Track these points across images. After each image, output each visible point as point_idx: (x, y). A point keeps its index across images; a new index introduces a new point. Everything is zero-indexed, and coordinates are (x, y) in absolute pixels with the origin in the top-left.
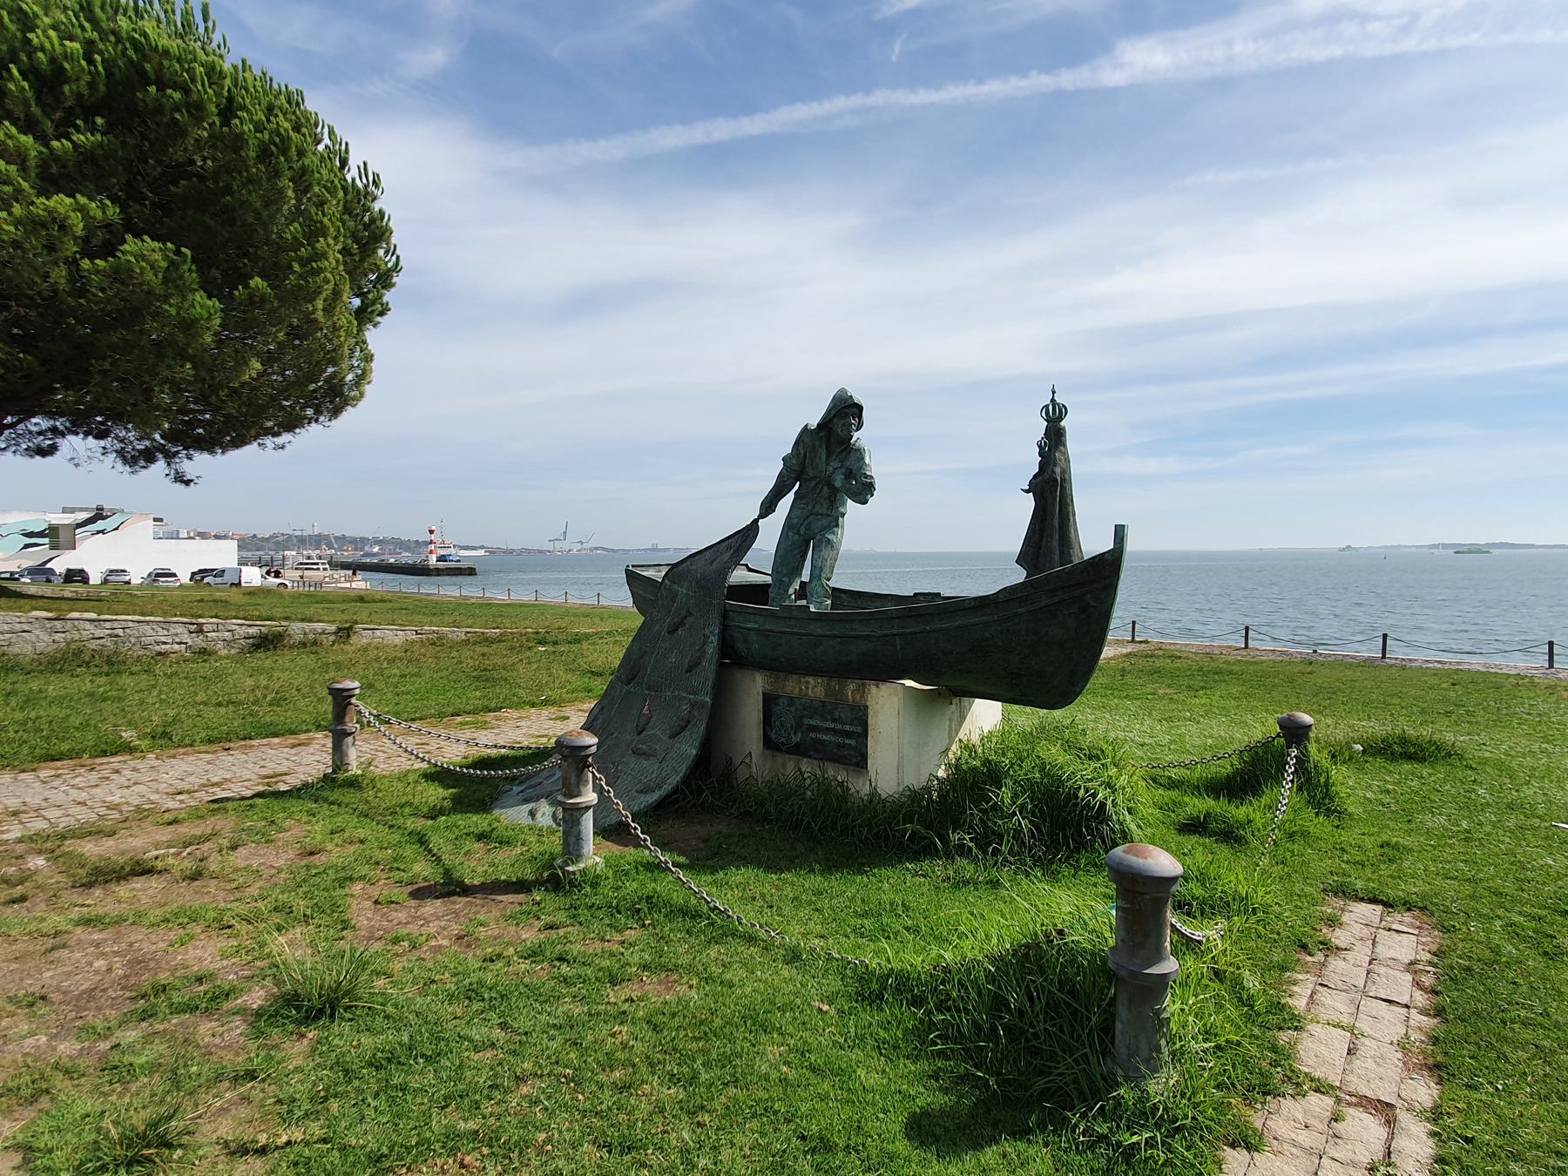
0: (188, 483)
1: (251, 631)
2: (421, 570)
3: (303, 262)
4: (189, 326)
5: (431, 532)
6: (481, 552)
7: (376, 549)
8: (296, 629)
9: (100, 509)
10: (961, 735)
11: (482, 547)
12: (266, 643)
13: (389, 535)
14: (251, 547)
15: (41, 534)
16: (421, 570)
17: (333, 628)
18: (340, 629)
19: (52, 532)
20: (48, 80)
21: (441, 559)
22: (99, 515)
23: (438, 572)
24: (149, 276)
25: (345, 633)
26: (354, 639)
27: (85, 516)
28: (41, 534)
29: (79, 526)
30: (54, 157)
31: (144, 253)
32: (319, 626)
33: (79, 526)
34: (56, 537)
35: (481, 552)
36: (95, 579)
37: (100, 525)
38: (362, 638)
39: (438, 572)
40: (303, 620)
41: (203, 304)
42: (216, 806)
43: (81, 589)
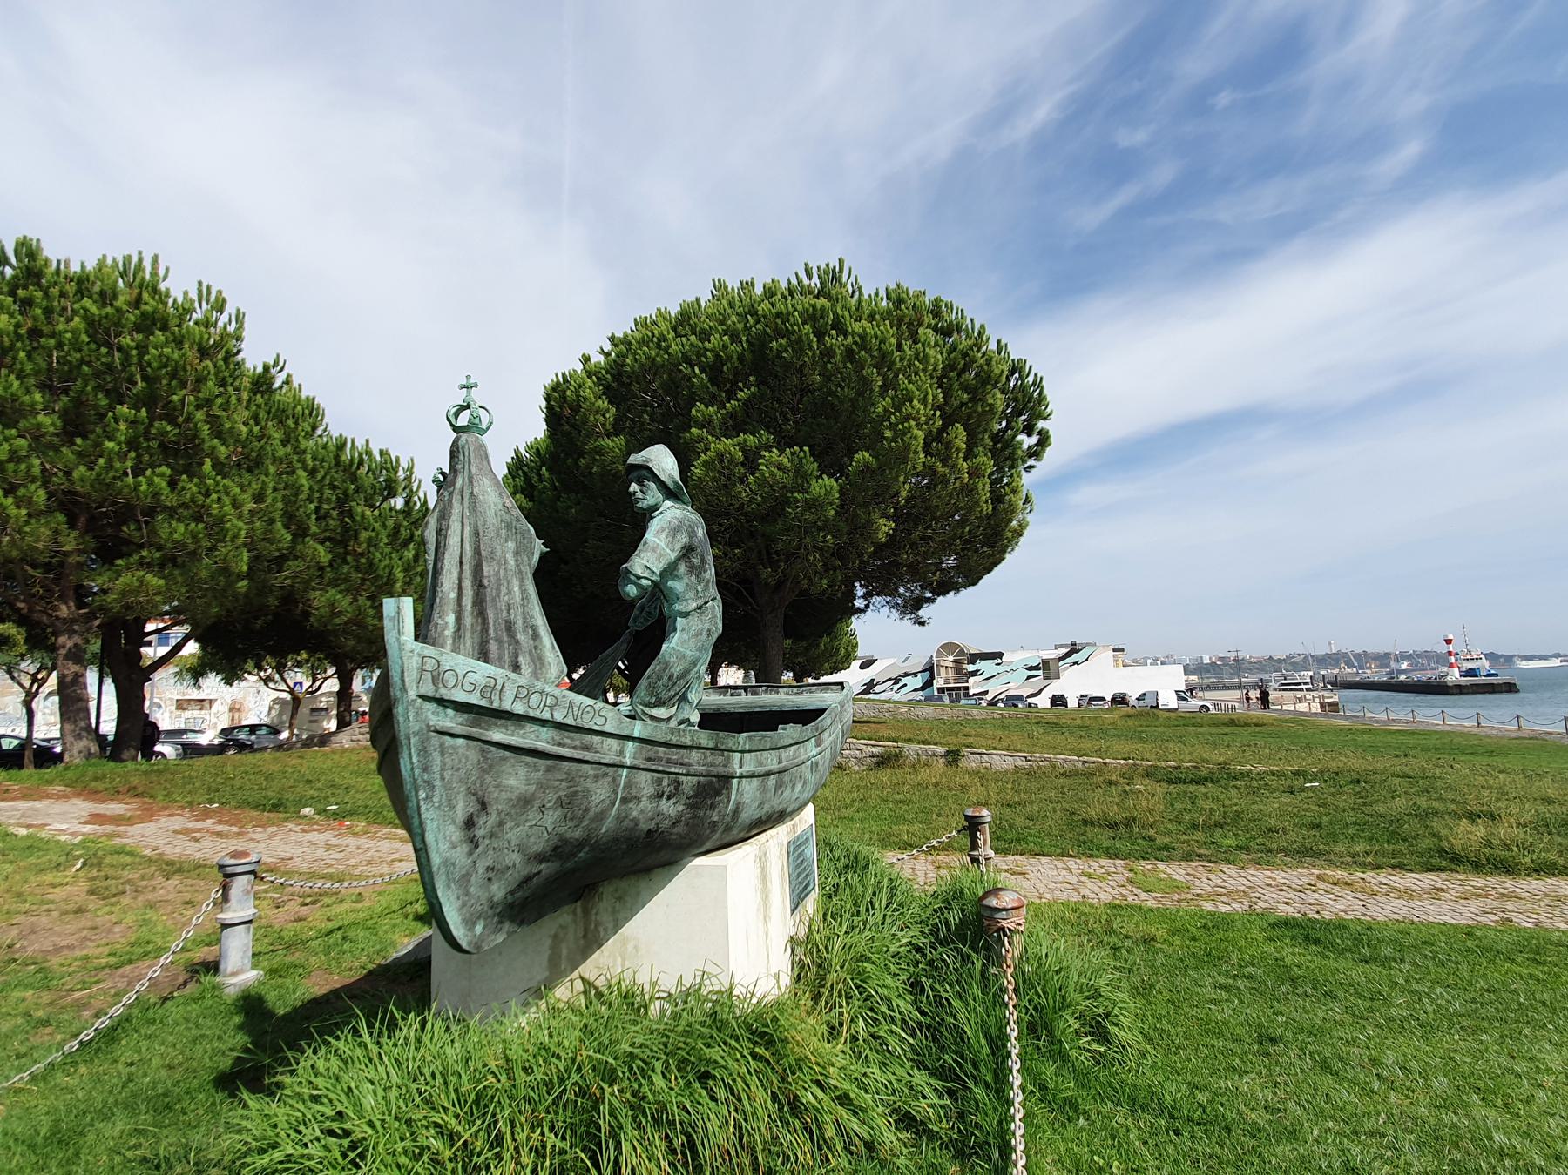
0: (922, 624)
1: (875, 750)
2: (1438, 688)
3: (893, 427)
4: (814, 505)
5: (1448, 642)
6: (1555, 663)
7: (1404, 665)
8: (910, 749)
9: (1074, 644)
10: (589, 969)
11: (1557, 656)
12: (883, 761)
13: (1419, 649)
14: (1205, 675)
15: (1037, 668)
16: (1438, 688)
17: (942, 750)
18: (948, 752)
19: (1045, 664)
20: (714, 370)
21: (1471, 673)
22: (1074, 649)
23: (1460, 690)
24: (779, 474)
25: (953, 757)
26: (963, 763)
27: (1064, 650)
28: (1037, 668)
29: (1061, 659)
30: (732, 415)
31: (776, 461)
32: (930, 748)
33: (1061, 659)
34: (1047, 669)
35: (1555, 663)
36: (1072, 703)
37: (1075, 657)
38: (970, 762)
39: (1460, 690)
40: (923, 743)
41: (825, 486)
42: (1293, 954)
43: (1124, 709)
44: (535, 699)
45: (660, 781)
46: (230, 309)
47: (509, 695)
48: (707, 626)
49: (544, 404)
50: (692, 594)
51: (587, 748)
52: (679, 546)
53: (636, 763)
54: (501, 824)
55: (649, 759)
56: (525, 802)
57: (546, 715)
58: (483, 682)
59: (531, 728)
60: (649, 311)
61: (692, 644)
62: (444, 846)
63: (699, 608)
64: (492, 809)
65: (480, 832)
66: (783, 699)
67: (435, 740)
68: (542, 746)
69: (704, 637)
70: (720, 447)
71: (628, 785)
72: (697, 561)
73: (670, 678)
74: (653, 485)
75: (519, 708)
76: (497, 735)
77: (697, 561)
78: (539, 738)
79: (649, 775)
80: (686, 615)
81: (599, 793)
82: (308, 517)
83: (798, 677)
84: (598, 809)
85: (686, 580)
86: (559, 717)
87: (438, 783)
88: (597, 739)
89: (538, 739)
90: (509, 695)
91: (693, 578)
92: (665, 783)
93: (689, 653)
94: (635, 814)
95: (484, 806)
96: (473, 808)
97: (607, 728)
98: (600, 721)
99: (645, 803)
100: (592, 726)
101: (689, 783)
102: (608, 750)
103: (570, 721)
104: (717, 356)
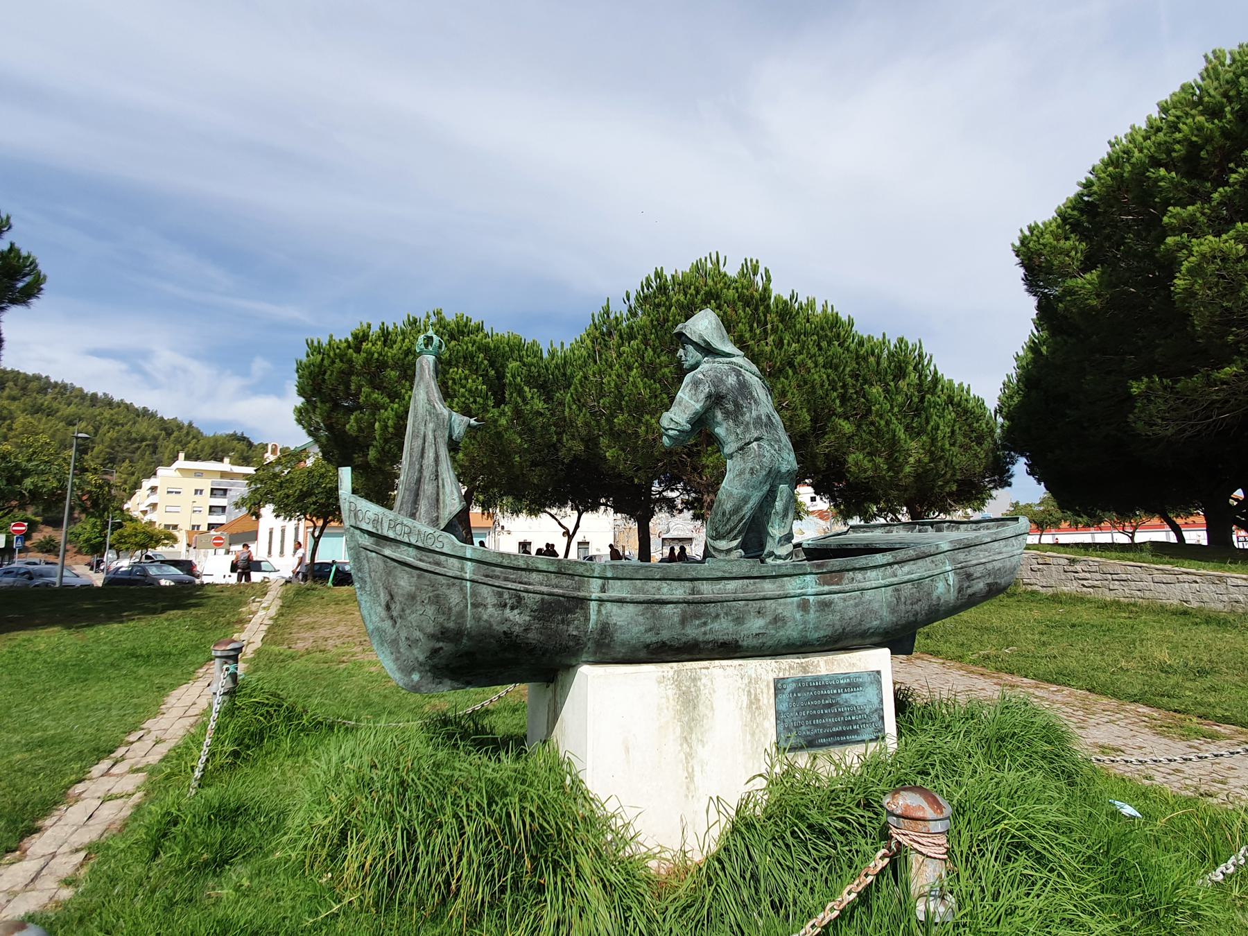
44: (398, 527)
45: (500, 595)
46: (761, 270)
47: (386, 525)
48: (750, 465)
49: (1017, 260)
50: (733, 437)
51: (438, 564)
52: (702, 396)
53: (475, 577)
54: (403, 610)
55: (487, 576)
56: (412, 597)
57: (407, 540)
58: (373, 517)
59: (885, 562)
60: (1122, 131)
61: (736, 483)
62: (375, 619)
63: (741, 449)
64: (396, 599)
65: (395, 614)
66: (876, 536)
67: (364, 553)
68: (410, 560)
69: (747, 476)
70: (1205, 248)
71: (474, 594)
72: (730, 407)
73: (724, 514)
74: (690, 348)
75: (391, 535)
76: (387, 552)
77: (730, 407)
78: (408, 556)
79: (489, 588)
80: (731, 456)
81: (454, 598)
82: (834, 401)
83: (914, 515)
84: (457, 609)
85: (725, 425)
86: (413, 541)
87: (368, 579)
88: (443, 558)
89: (408, 555)
90: (386, 525)
91: (731, 422)
92: (506, 596)
93: (735, 491)
94: (485, 617)
95: (392, 597)
96: (388, 598)
97: (445, 550)
98: (440, 545)
99: (491, 610)
100: (433, 548)
101: (530, 599)
102: (452, 566)
103: (420, 544)
104: (1192, 144)
